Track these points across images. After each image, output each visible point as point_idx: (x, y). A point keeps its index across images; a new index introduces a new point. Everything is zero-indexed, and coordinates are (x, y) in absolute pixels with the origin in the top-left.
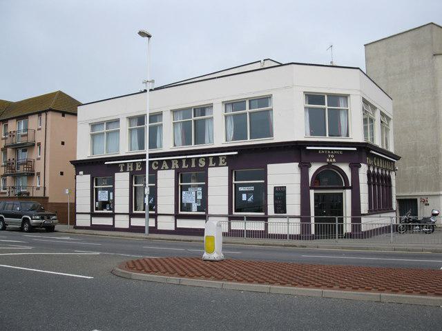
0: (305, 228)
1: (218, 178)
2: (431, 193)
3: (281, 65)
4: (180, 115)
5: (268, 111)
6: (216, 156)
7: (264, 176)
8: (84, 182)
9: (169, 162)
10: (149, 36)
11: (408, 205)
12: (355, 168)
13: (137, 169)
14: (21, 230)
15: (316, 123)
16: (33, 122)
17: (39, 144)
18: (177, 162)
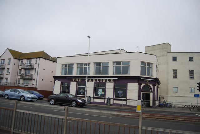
1: (110, 86)
3: (128, 53)
6: (109, 79)
8: (58, 84)
12: (154, 86)
13: (80, 81)
15: (143, 71)
16: (33, 61)
17: (35, 69)
18: (95, 80)
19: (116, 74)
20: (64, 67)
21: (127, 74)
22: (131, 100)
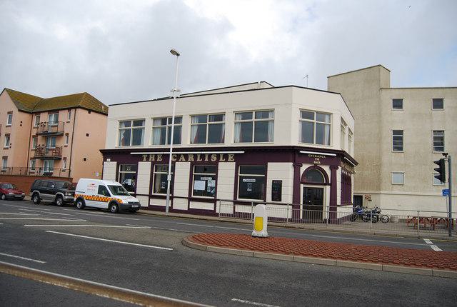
0: (295, 214)
1: (227, 171)
2: (373, 192)
3: (274, 88)
4: (196, 120)
5: (141, 129)
6: (225, 153)
7: (265, 171)
9: (186, 156)
10: (178, 55)
11: (359, 199)
12: (334, 169)
14: (54, 204)
15: (306, 133)
16: (63, 116)
17: (67, 134)
19: (243, 140)
20: (159, 125)
21: (140, 144)
22: (226, 201)
